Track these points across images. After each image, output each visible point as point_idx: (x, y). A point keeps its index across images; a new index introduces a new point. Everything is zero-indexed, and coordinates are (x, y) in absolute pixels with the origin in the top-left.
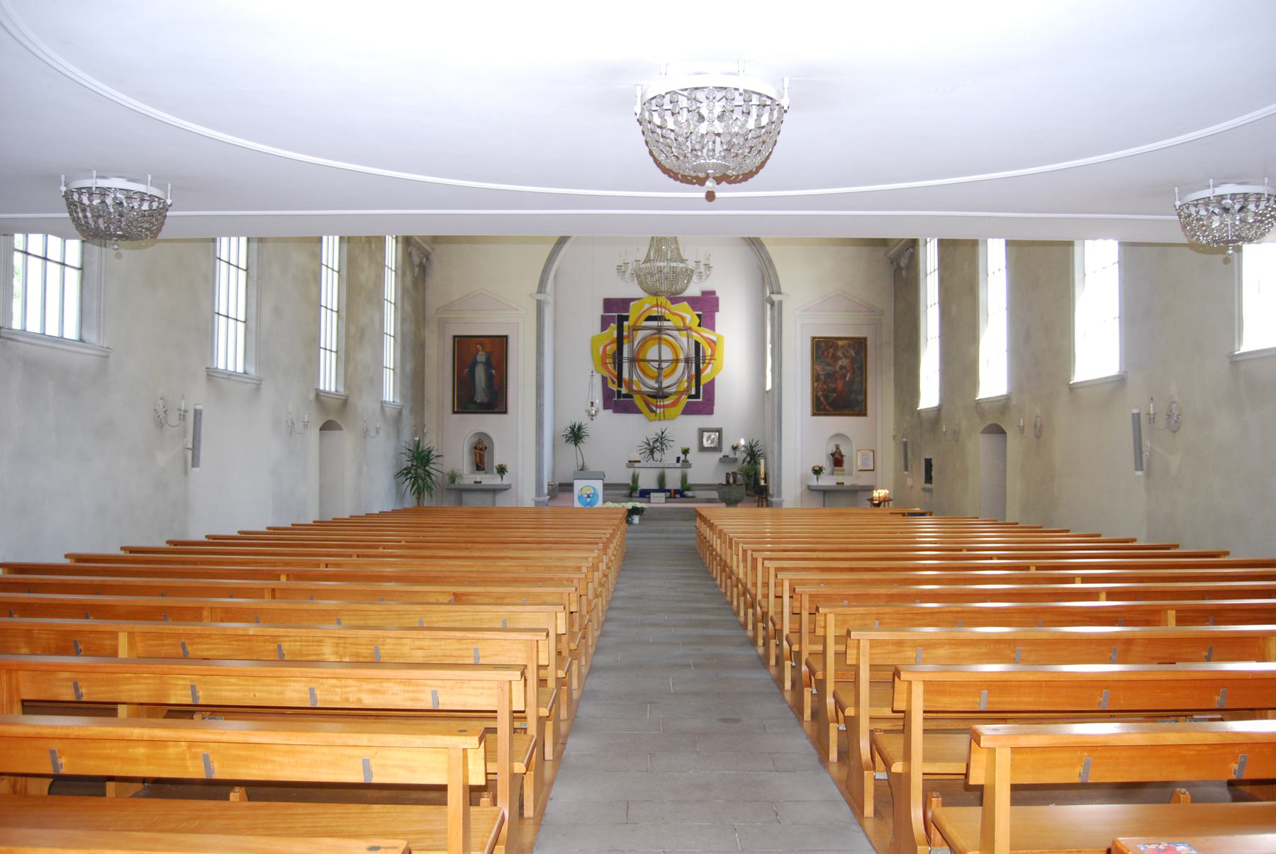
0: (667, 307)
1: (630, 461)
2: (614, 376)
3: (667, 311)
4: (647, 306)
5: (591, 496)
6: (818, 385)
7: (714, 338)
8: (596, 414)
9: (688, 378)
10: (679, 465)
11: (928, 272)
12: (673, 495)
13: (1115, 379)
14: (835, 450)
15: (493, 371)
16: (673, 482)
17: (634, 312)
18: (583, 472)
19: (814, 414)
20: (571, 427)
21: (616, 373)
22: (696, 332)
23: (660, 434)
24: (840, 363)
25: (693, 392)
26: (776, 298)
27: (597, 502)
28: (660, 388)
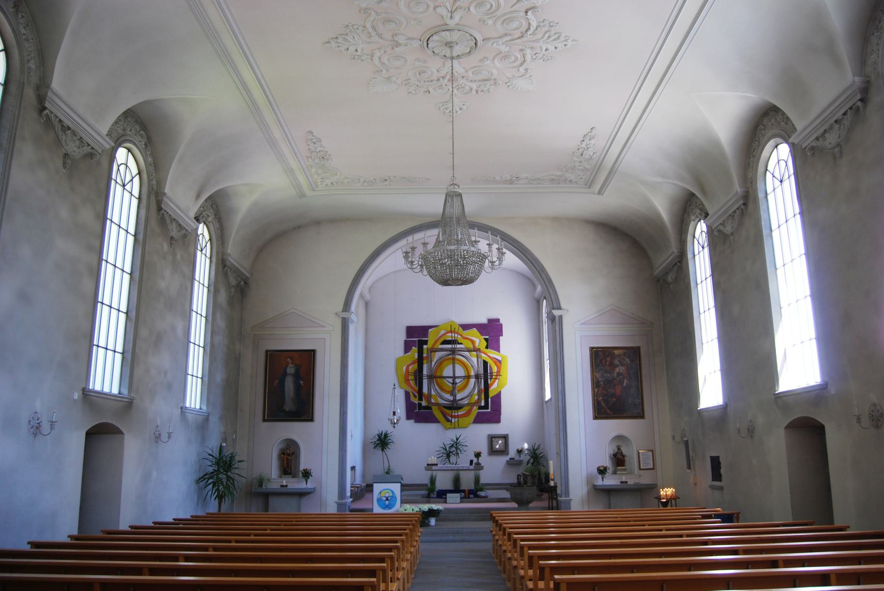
0: (459, 332)
1: (428, 465)
2: (416, 391)
3: (459, 336)
4: (443, 332)
5: (389, 498)
6: (598, 390)
7: (500, 358)
8: (397, 423)
9: (478, 391)
10: (472, 467)
11: (699, 281)
12: (467, 496)
13: (721, 407)
14: (616, 450)
15: (301, 382)
16: (467, 482)
17: (432, 338)
18: (388, 476)
19: (596, 418)
20: (378, 435)
21: (417, 388)
22: (484, 353)
23: (456, 440)
24: (617, 370)
25: (483, 404)
26: (556, 313)
27: (394, 506)
28: (455, 400)
